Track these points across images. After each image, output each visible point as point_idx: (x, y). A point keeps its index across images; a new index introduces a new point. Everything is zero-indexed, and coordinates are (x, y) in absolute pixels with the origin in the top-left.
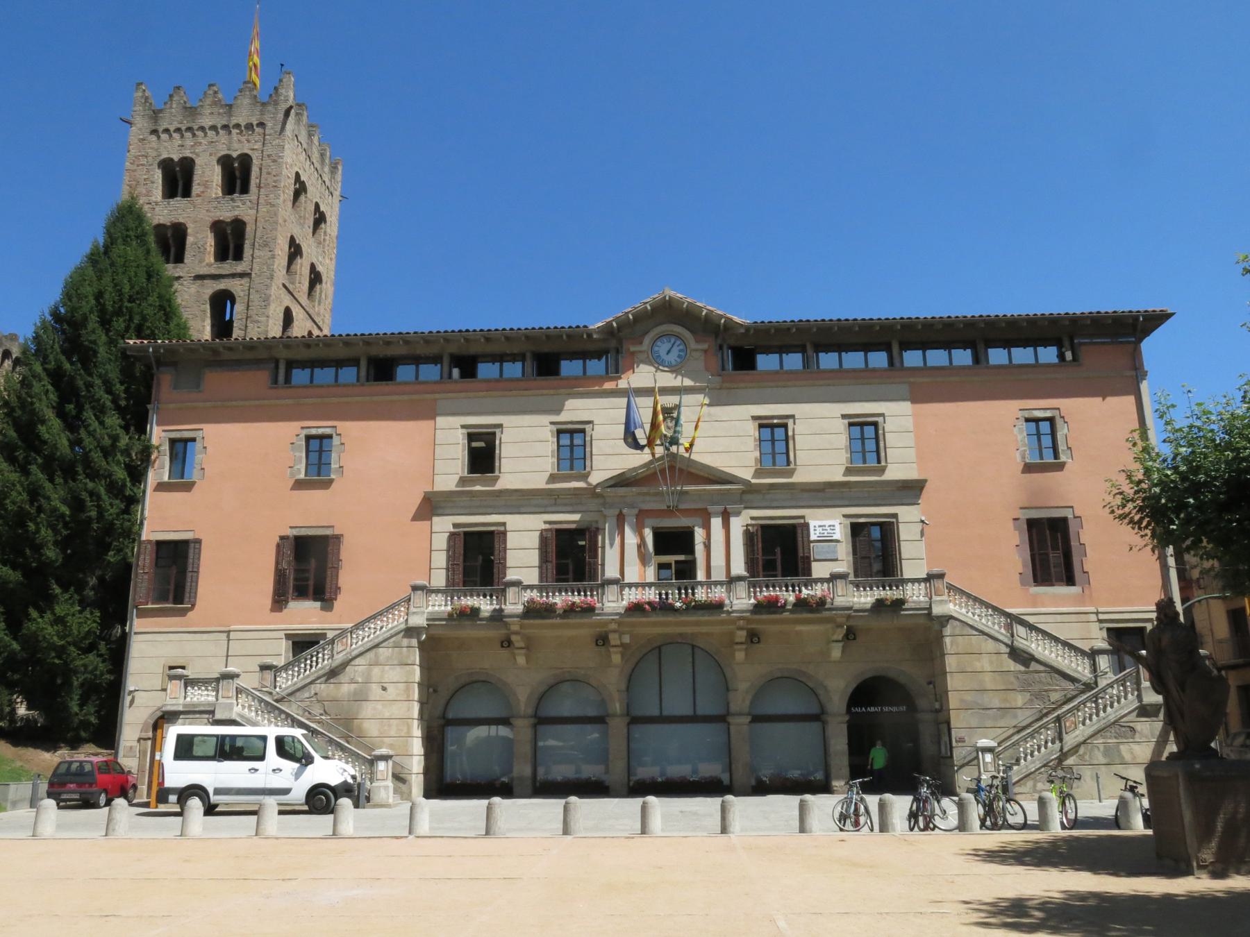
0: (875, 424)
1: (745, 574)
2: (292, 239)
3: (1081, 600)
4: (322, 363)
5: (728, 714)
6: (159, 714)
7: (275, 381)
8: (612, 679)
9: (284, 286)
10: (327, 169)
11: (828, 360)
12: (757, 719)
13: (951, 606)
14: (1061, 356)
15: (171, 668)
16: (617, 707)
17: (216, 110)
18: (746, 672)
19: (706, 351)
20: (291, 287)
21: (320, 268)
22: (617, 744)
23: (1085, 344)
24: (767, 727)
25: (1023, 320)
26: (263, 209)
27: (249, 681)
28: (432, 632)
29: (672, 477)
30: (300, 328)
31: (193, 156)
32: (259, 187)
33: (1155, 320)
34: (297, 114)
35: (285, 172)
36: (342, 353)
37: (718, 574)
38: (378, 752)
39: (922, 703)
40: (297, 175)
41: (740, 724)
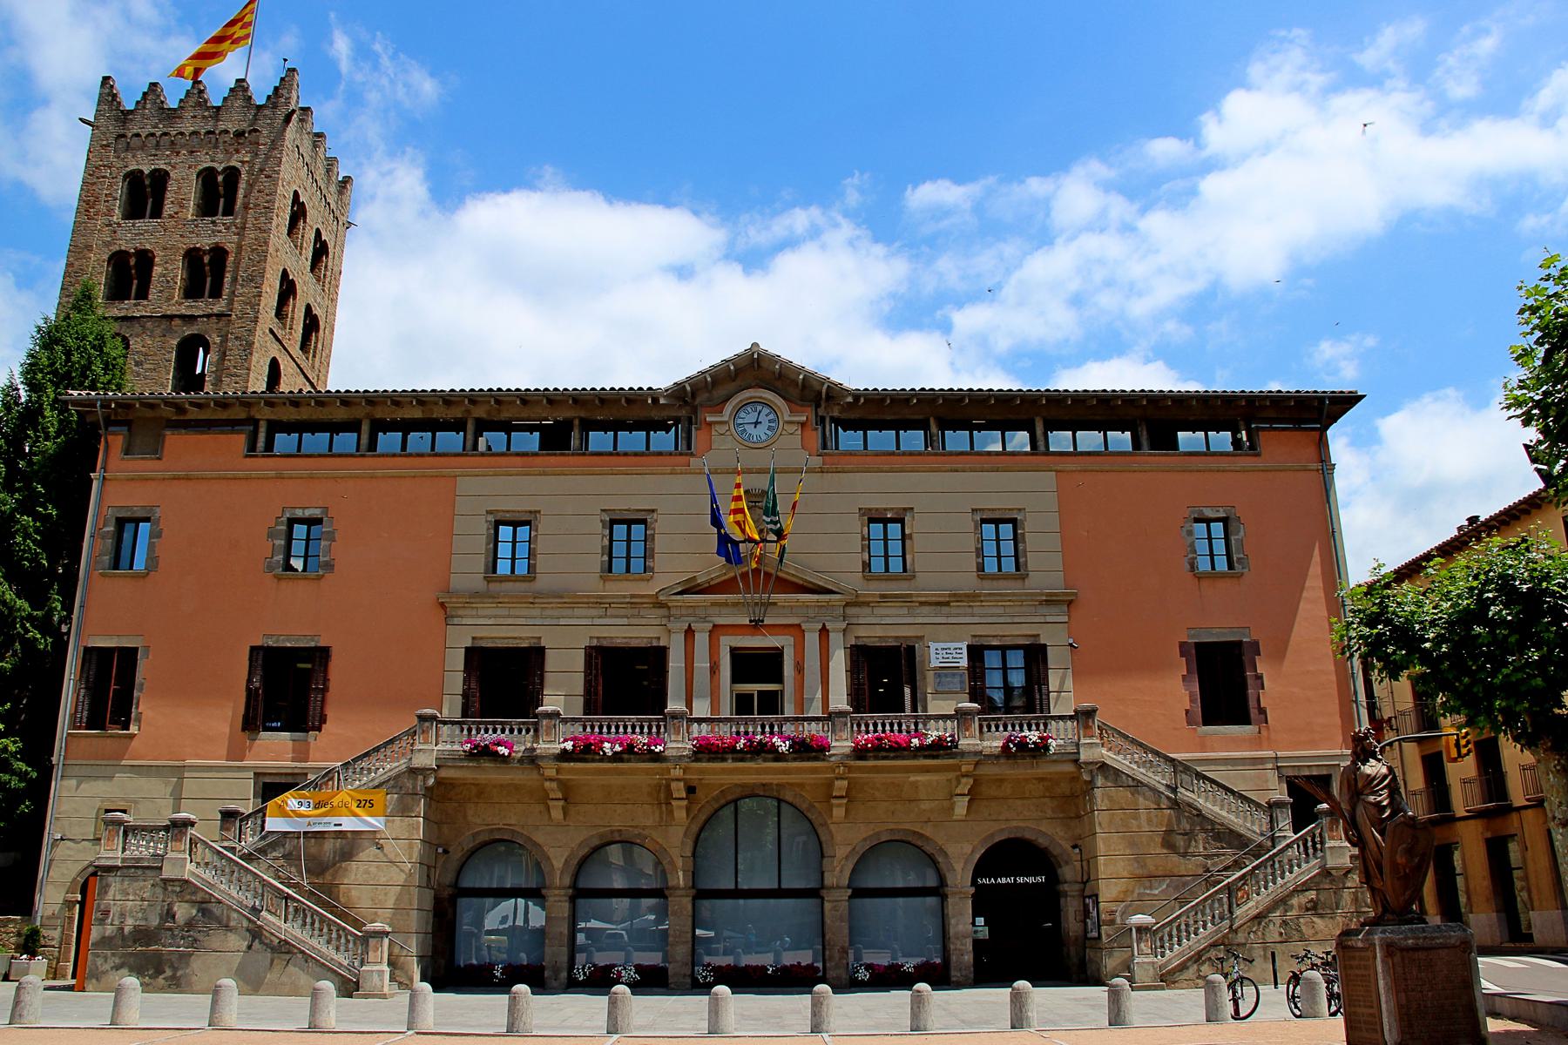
0: (1014, 521)
1: (849, 708)
2: (285, 273)
3: (1257, 743)
4: (314, 427)
5: (823, 887)
6: (91, 870)
7: (252, 447)
8: (675, 840)
9: (271, 331)
10: (333, 188)
11: (956, 440)
12: (859, 893)
13: (1104, 751)
14: (1237, 443)
15: (107, 811)
16: (680, 879)
17: (199, 112)
18: (846, 839)
19: (803, 425)
20: (280, 334)
21: (317, 311)
22: (677, 923)
23: (1264, 429)
24: (868, 902)
25: (1118, 397)
26: (251, 235)
27: (207, 829)
28: (443, 773)
29: (756, 585)
30: (290, 383)
31: (168, 168)
32: (246, 207)
33: (1346, 401)
34: (301, 120)
35: (280, 190)
36: (341, 414)
37: (816, 711)
38: (369, 927)
39: (1068, 872)
40: (296, 194)
41: (837, 903)
